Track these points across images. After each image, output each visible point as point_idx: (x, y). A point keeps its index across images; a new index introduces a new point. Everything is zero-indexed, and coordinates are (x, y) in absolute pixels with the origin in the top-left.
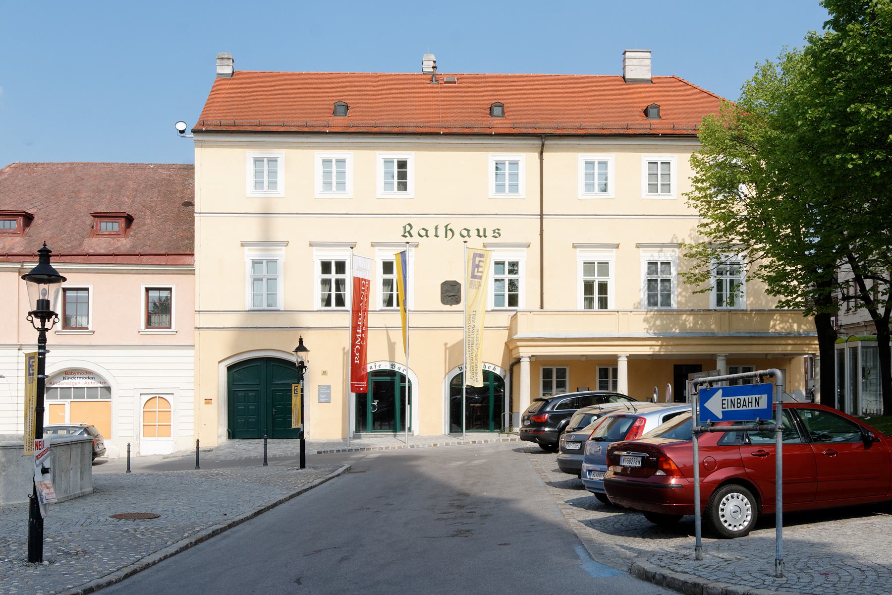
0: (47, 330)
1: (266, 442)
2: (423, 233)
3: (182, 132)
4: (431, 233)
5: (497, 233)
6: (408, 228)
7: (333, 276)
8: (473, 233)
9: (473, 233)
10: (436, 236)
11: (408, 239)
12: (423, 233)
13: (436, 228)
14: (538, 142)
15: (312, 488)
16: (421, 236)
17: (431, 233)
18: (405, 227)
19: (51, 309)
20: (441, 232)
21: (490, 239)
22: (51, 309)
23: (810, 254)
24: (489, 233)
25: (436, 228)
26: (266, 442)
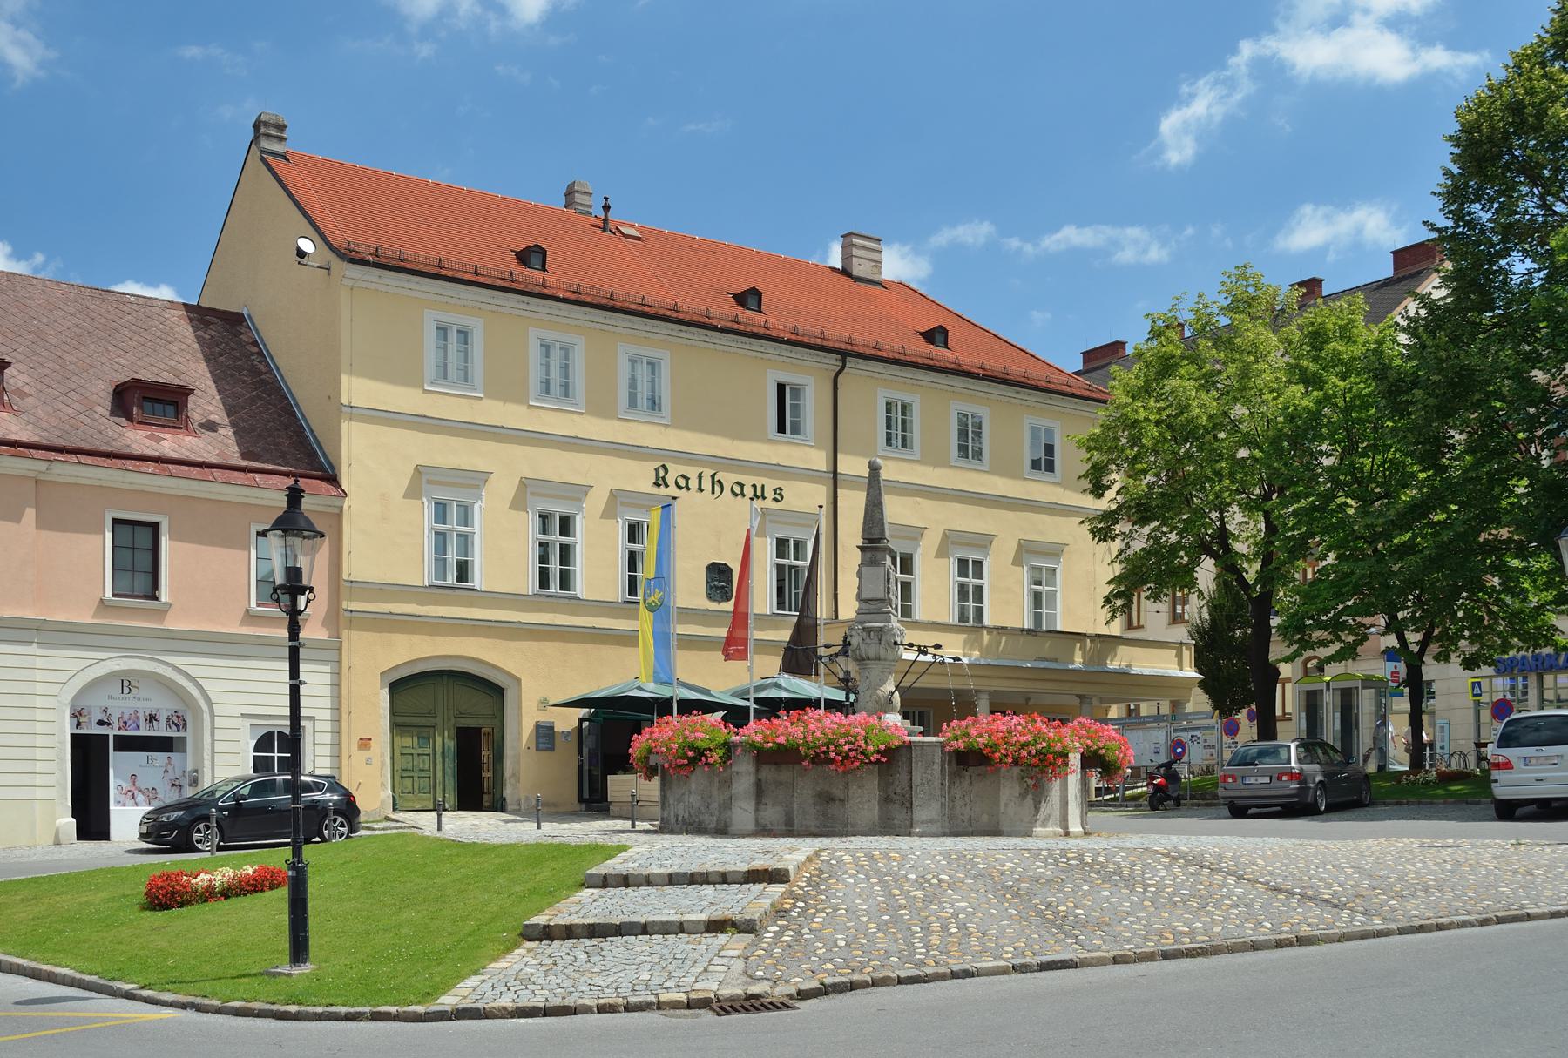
0: (300, 612)
1: (439, 816)
2: (682, 482)
3: (301, 254)
4: (693, 484)
5: (779, 495)
6: (662, 473)
8: (749, 491)
9: (749, 491)
10: (701, 490)
11: (662, 490)
12: (682, 482)
13: (700, 477)
14: (832, 361)
15: (967, 974)
16: (680, 488)
17: (693, 484)
18: (657, 470)
19: (305, 583)
21: (769, 503)
22: (305, 583)
23: (1445, 510)
24: (769, 493)
25: (700, 477)
26: (439, 816)
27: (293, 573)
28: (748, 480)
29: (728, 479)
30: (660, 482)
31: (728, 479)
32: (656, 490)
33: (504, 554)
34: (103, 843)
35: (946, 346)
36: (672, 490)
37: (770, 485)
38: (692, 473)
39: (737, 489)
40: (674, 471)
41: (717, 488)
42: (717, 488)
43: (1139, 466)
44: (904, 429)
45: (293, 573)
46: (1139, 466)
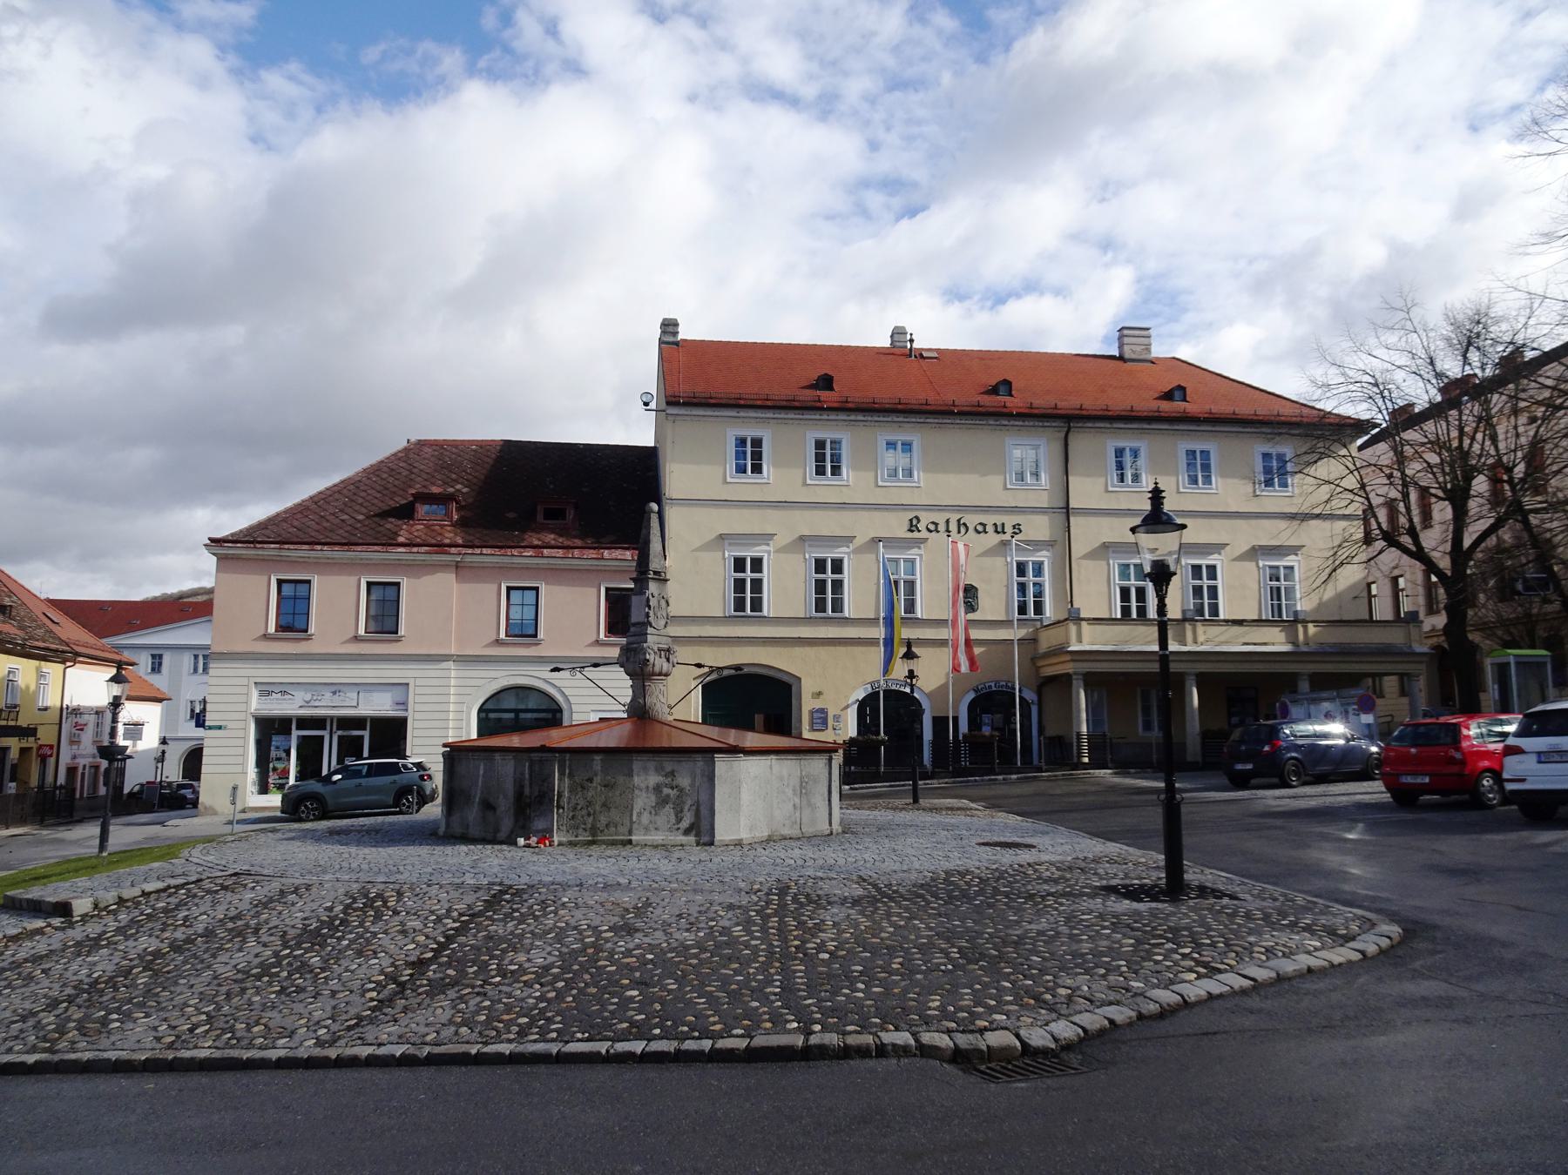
2: (932, 527)
4: (942, 527)
5: (1017, 529)
7: (749, 575)
8: (990, 528)
9: (990, 528)
11: (916, 535)
12: (932, 527)
13: (948, 522)
17: (942, 527)
20: (953, 527)
24: (1009, 529)
27: (911, 672)
28: (990, 520)
29: (972, 520)
30: (913, 527)
31: (972, 520)
32: (910, 535)
33: (785, 588)
34: (255, 789)
35: (1185, 400)
36: (924, 534)
37: (1009, 521)
38: (941, 518)
39: (980, 528)
40: (926, 518)
41: (963, 530)
42: (963, 530)
43: (1480, 484)
44: (1280, 606)
45: (911, 672)
46: (1480, 484)
